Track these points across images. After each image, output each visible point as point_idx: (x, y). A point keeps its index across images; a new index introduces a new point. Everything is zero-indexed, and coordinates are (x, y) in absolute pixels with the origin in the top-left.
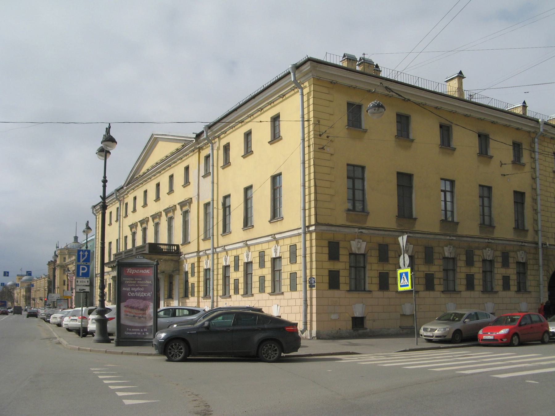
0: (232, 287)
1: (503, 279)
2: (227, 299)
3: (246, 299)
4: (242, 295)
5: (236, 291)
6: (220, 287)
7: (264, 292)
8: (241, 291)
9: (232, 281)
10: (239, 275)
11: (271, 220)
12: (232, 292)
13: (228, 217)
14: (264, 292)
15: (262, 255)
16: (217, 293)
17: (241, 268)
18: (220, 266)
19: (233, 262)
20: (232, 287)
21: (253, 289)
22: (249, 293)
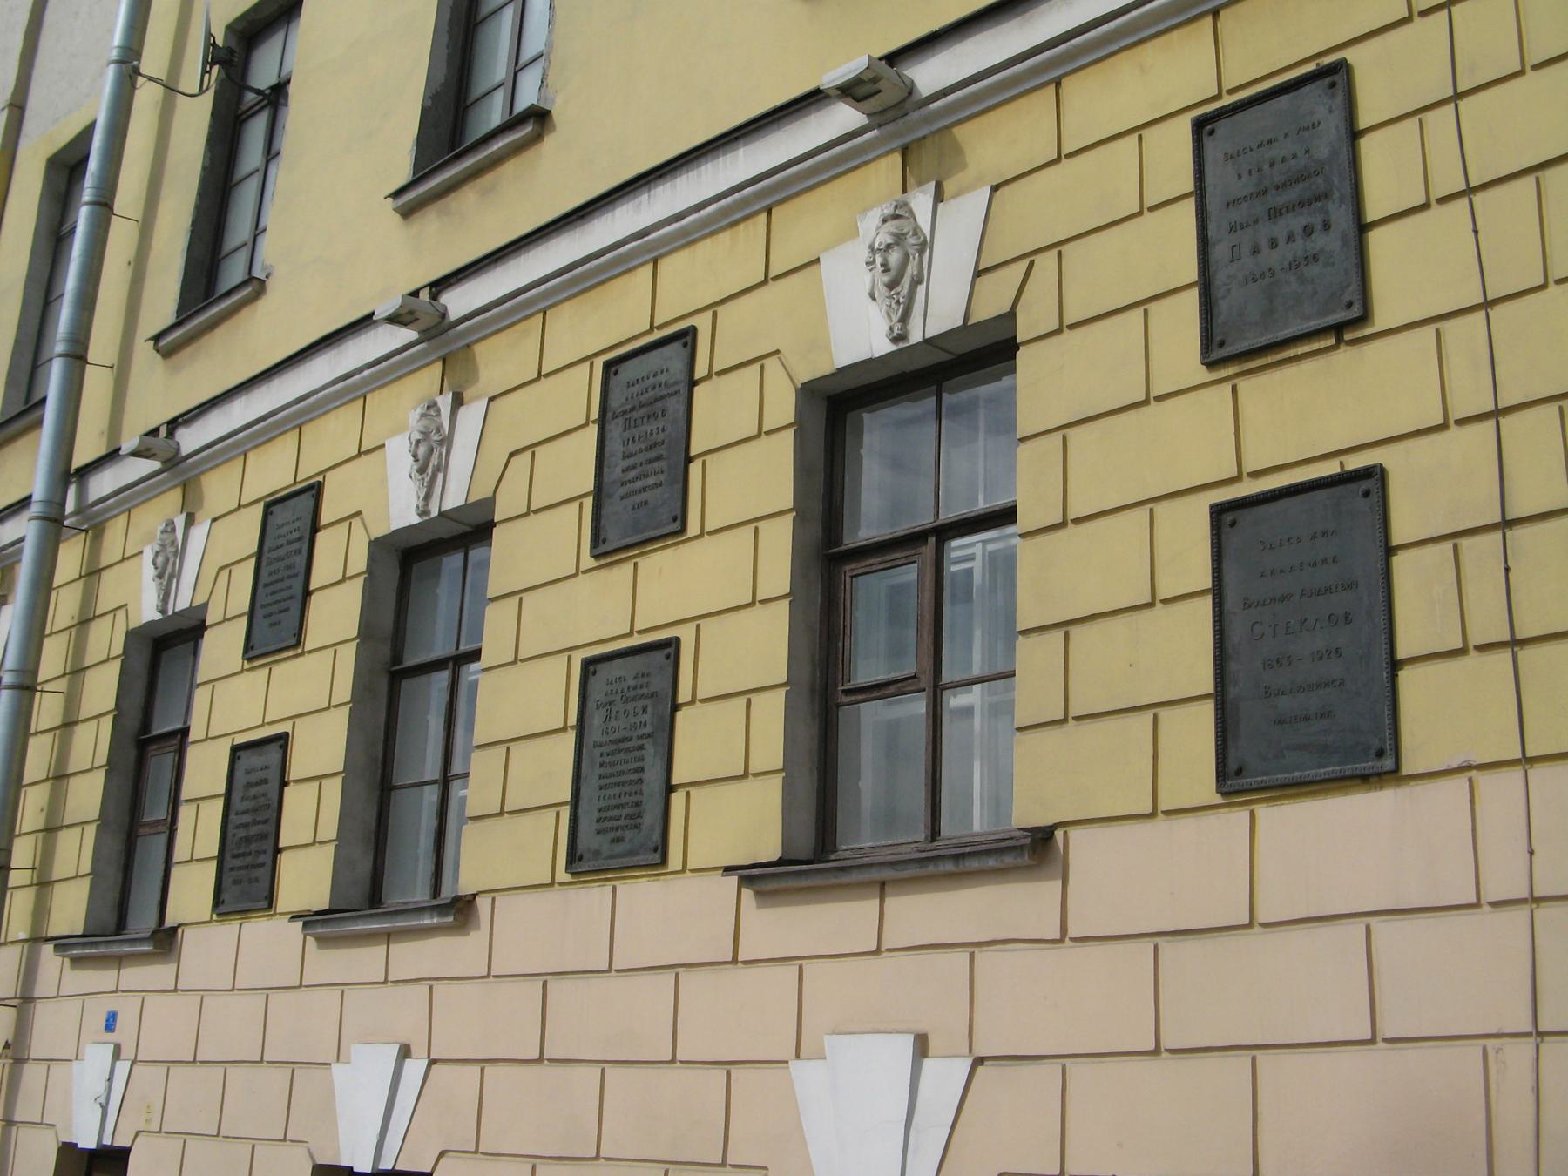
0: (200, 830)
1: (243, 913)
2: (134, 976)
3: (365, 960)
4: (310, 920)
5: (246, 881)
6: (76, 851)
7: (265, 901)
8: (306, 877)
9: (206, 771)
10: (308, 699)
11: (423, 170)
12: (191, 890)
13: (246, 195)
14: (265, 901)
15: (294, 518)
16: (41, 911)
17: (336, 613)
18: (107, 640)
19: (244, 576)
20: (200, 830)
21: (176, 873)
22: (142, 920)
